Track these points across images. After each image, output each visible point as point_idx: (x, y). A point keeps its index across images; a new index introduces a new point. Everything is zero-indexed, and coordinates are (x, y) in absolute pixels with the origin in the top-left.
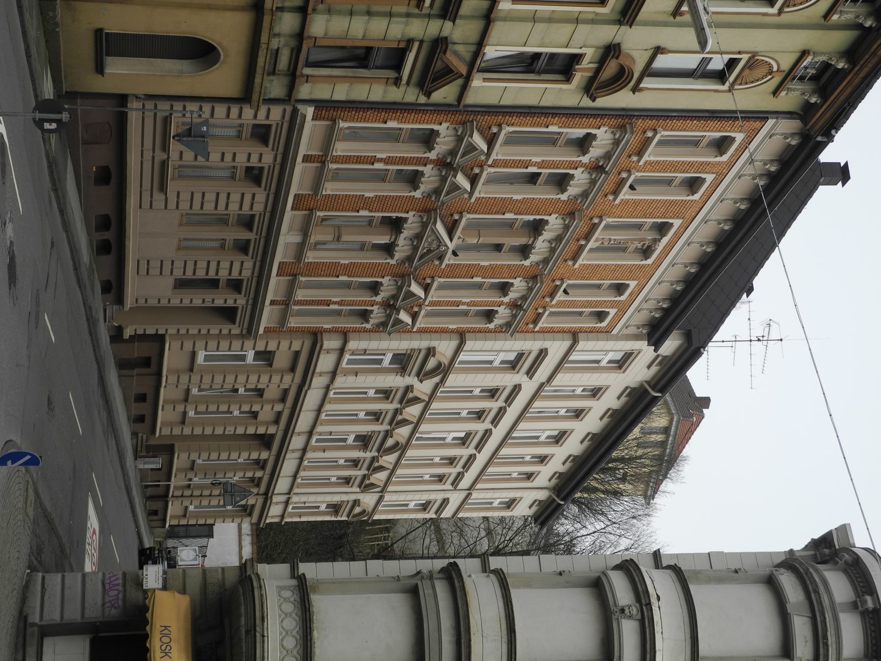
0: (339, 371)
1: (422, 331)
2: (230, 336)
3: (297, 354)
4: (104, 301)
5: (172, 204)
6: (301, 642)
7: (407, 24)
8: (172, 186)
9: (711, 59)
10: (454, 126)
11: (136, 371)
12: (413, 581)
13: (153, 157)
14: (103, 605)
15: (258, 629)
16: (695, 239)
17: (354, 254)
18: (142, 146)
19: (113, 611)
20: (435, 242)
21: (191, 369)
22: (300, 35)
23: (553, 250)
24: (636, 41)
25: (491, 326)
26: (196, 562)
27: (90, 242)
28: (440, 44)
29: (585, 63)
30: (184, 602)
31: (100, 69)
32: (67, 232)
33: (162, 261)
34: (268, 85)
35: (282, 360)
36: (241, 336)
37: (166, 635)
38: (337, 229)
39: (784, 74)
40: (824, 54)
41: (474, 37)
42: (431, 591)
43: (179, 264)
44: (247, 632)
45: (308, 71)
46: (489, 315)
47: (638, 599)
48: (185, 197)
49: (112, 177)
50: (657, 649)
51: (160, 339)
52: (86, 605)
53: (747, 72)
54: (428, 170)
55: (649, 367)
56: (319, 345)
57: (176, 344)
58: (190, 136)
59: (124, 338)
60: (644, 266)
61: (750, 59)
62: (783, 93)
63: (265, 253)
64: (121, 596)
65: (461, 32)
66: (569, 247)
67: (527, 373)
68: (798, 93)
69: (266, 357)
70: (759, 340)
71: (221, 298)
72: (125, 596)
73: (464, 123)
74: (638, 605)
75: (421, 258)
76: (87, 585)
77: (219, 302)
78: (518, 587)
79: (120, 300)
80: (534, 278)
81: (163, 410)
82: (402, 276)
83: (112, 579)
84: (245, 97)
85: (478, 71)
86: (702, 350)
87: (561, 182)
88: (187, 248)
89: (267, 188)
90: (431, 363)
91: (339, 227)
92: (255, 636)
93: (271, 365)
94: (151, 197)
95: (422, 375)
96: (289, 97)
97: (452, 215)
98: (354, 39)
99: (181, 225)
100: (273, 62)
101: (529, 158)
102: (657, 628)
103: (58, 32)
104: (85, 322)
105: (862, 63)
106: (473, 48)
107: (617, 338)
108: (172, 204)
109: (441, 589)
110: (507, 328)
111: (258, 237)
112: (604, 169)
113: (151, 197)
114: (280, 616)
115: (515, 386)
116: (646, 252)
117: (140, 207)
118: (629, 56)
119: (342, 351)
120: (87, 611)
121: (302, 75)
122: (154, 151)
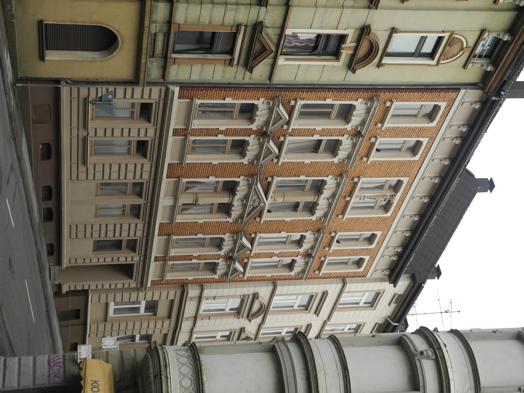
0: (198, 316)
1: (251, 280)
2: (130, 289)
3: (172, 301)
4: (49, 262)
5: (91, 176)
6: (195, 382)
7: (236, 11)
8: (91, 160)
9: (427, 37)
10: (267, 101)
11: (70, 322)
12: (272, 344)
13: (78, 134)
14: (49, 376)
15: (163, 373)
16: (417, 194)
17: (206, 216)
18: (71, 125)
19: (57, 380)
20: (257, 200)
21: (106, 320)
22: (169, 22)
23: (330, 205)
24: (380, 21)
25: (292, 274)
26: (116, 347)
27: (39, 209)
28: (257, 27)
29: (349, 43)
30: (108, 367)
31: (42, 58)
32: (23, 178)
33: (85, 225)
34: (150, 66)
35: (162, 309)
36: (137, 289)
37: (95, 387)
38: (195, 195)
39: (471, 49)
40: (495, 31)
41: (279, 22)
42: (284, 348)
43: (96, 228)
44: (155, 377)
45: (174, 56)
46: (291, 266)
47: (431, 345)
48: (99, 168)
49: (51, 152)
50: (450, 378)
51: (85, 293)
52: (37, 376)
53: (448, 48)
54: (252, 140)
55: (389, 305)
56: (186, 292)
57: (96, 297)
58: (101, 101)
59: (63, 293)
60: (385, 219)
61: (450, 36)
62: (470, 66)
63: (150, 216)
64: (62, 369)
65: (270, 16)
66: (340, 203)
67: (315, 313)
68: (479, 65)
69: (152, 307)
70: (446, 312)
71: (124, 257)
72: (65, 369)
73: (273, 99)
74: (432, 349)
75: (248, 215)
76: (37, 364)
77: (122, 261)
78: (346, 347)
79: (59, 262)
80: (318, 231)
81: (89, 336)
82: (237, 233)
83: (55, 359)
84: (134, 82)
85: (281, 54)
86: (423, 285)
87: (333, 147)
88: (101, 216)
89: (151, 160)
90: (256, 307)
91: (196, 194)
92: (161, 379)
93: (155, 315)
94: (78, 170)
95: (250, 316)
96: (163, 81)
97: (267, 179)
98: (203, 26)
99: (97, 195)
100: (152, 46)
101: (314, 127)
102: (448, 364)
103: (13, 23)
104: (37, 260)
105: (519, 33)
106: (278, 31)
107: (370, 281)
108: (91, 176)
109: (293, 348)
110: (302, 276)
111: (146, 202)
112: (361, 133)
113: (78, 170)
114: (178, 365)
115: (308, 325)
116: (386, 208)
117: (71, 179)
118: (375, 35)
119: (200, 298)
120: (37, 380)
121: (171, 58)
122: (78, 130)
